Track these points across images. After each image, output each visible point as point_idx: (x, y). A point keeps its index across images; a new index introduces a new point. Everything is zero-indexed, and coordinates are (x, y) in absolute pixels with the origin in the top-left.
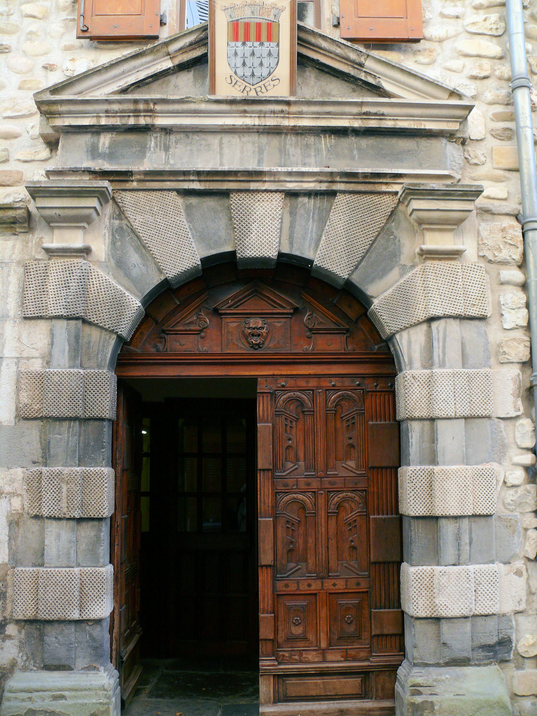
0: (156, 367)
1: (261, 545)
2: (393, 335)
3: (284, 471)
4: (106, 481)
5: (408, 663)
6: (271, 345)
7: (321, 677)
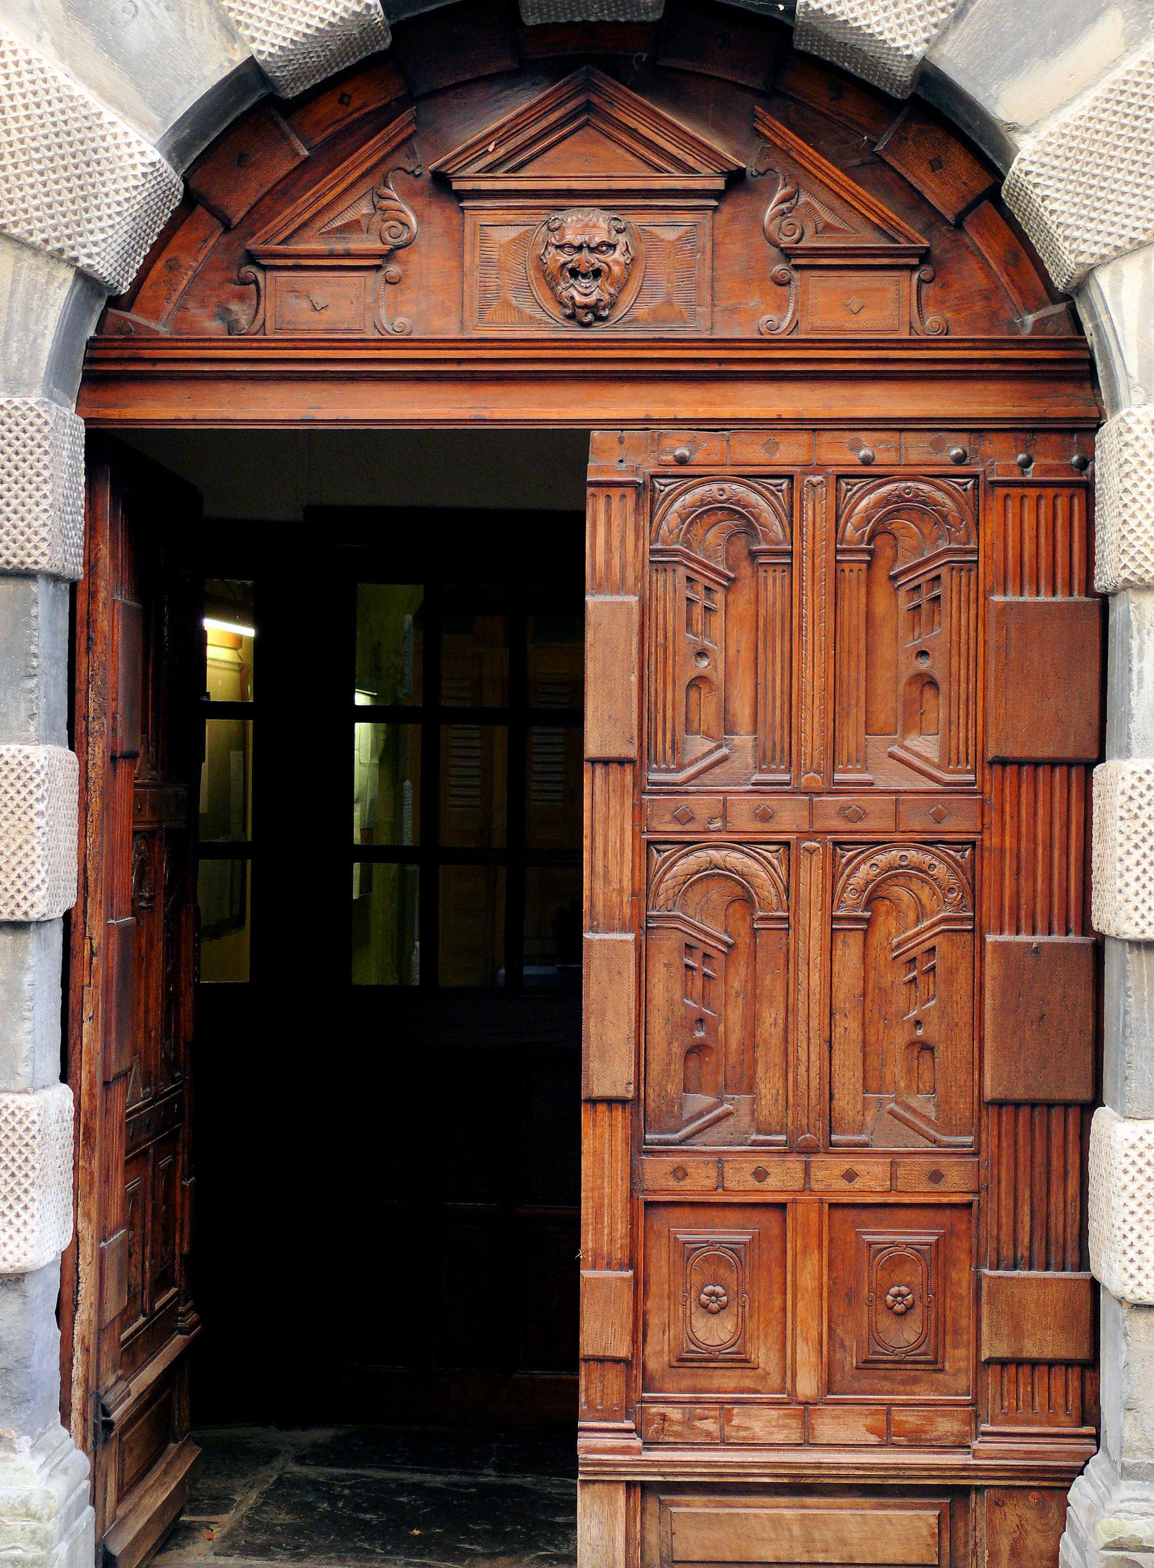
0: (225, 387)
1: (591, 1027)
2: (1090, 271)
3: (681, 768)
4: (38, 794)
5: (1106, 1466)
6: (641, 311)
7: (796, 1500)
